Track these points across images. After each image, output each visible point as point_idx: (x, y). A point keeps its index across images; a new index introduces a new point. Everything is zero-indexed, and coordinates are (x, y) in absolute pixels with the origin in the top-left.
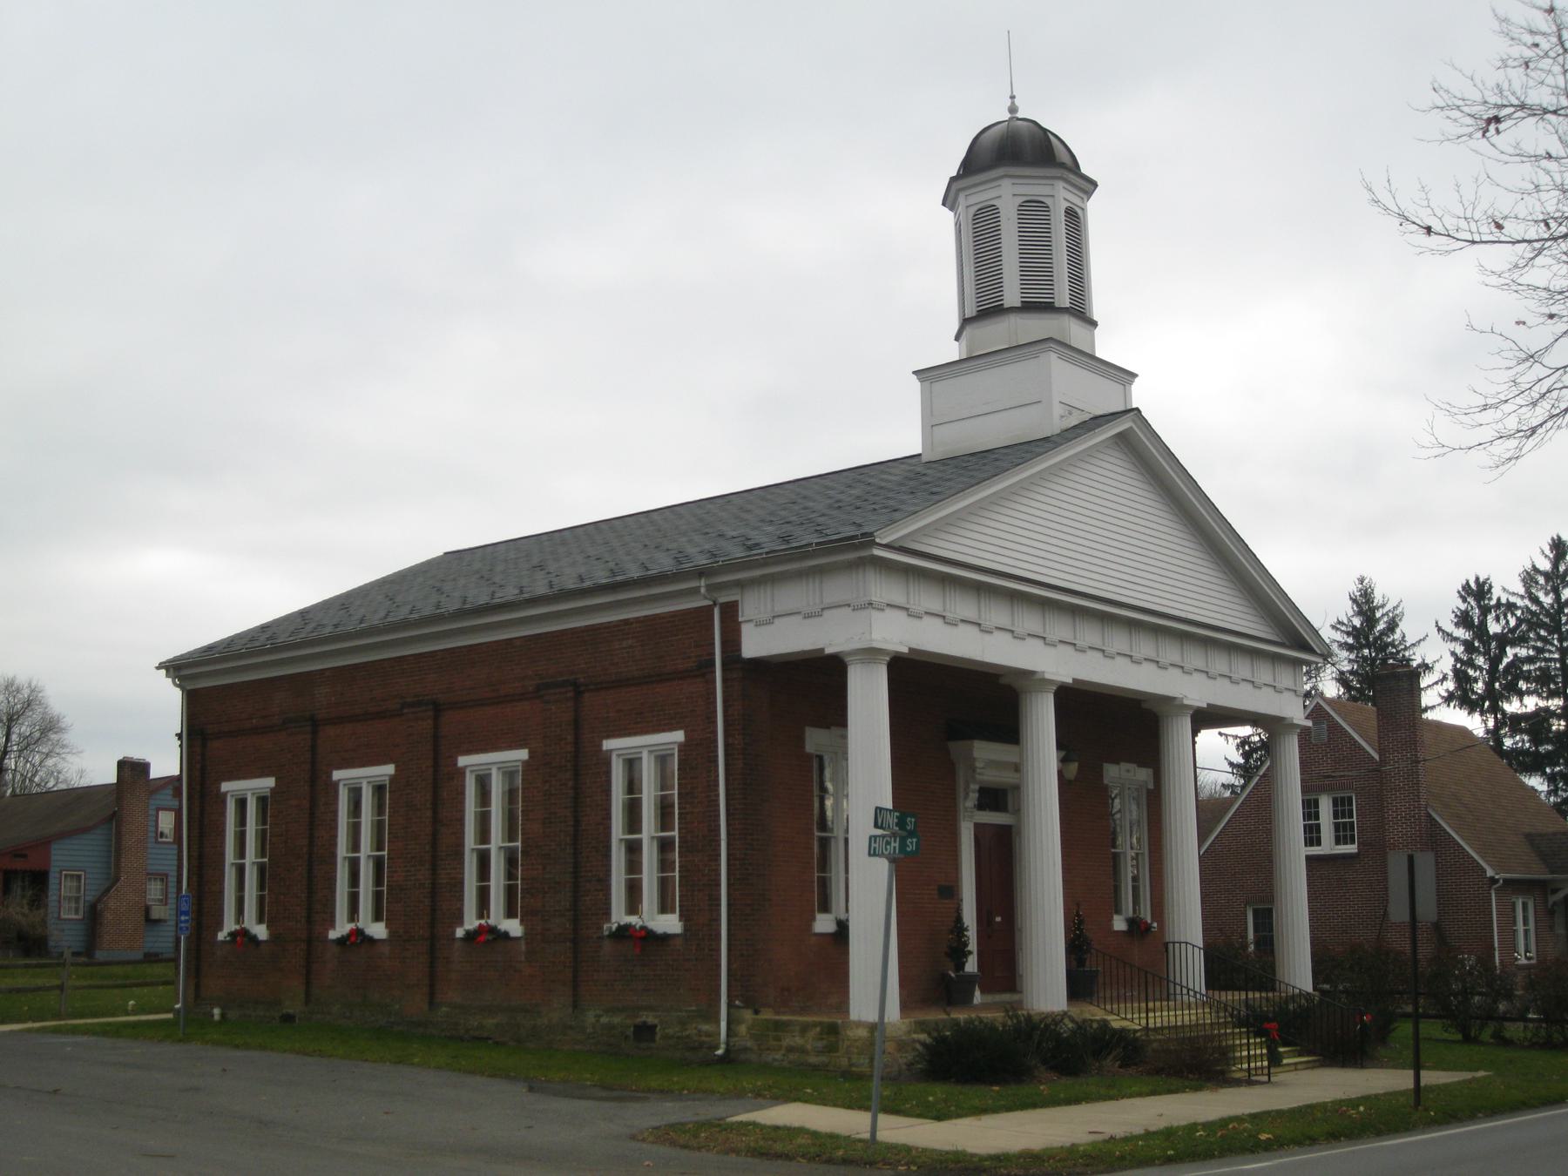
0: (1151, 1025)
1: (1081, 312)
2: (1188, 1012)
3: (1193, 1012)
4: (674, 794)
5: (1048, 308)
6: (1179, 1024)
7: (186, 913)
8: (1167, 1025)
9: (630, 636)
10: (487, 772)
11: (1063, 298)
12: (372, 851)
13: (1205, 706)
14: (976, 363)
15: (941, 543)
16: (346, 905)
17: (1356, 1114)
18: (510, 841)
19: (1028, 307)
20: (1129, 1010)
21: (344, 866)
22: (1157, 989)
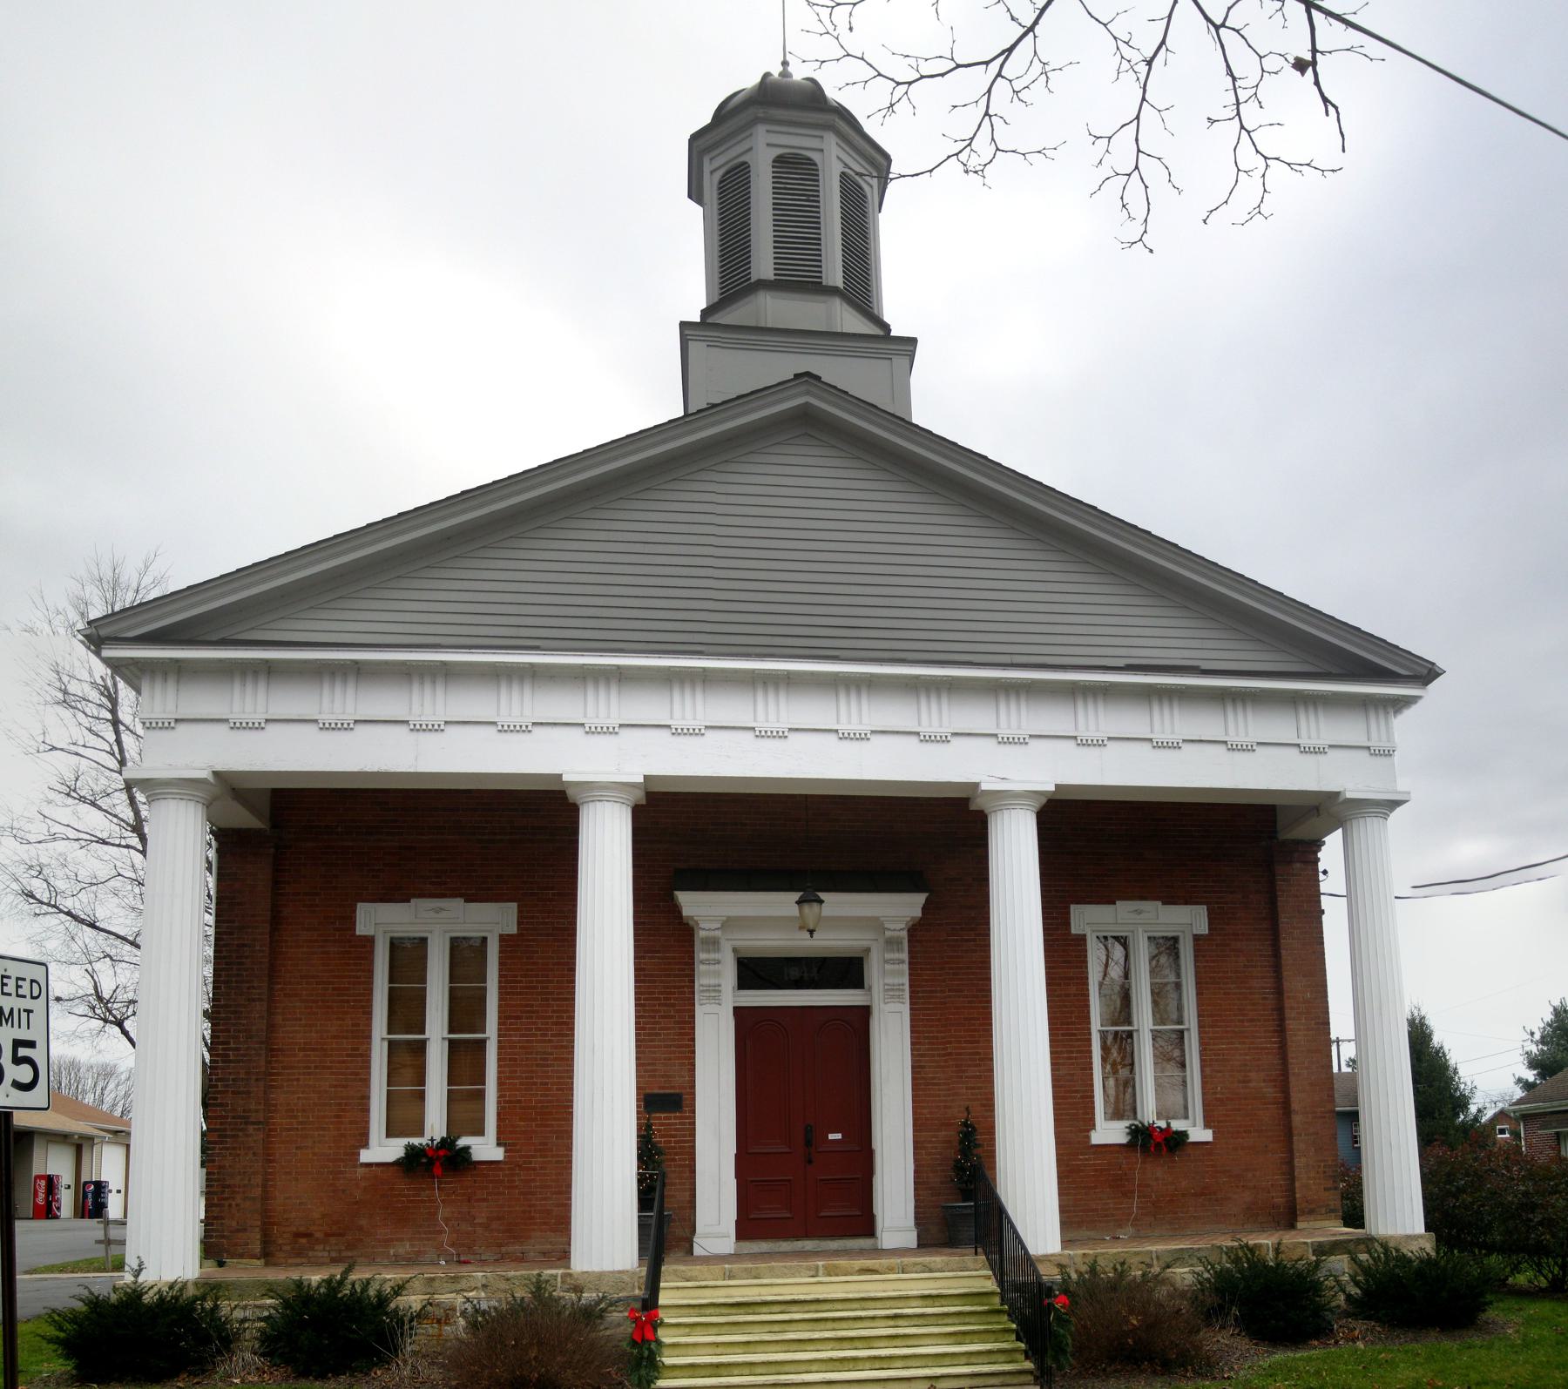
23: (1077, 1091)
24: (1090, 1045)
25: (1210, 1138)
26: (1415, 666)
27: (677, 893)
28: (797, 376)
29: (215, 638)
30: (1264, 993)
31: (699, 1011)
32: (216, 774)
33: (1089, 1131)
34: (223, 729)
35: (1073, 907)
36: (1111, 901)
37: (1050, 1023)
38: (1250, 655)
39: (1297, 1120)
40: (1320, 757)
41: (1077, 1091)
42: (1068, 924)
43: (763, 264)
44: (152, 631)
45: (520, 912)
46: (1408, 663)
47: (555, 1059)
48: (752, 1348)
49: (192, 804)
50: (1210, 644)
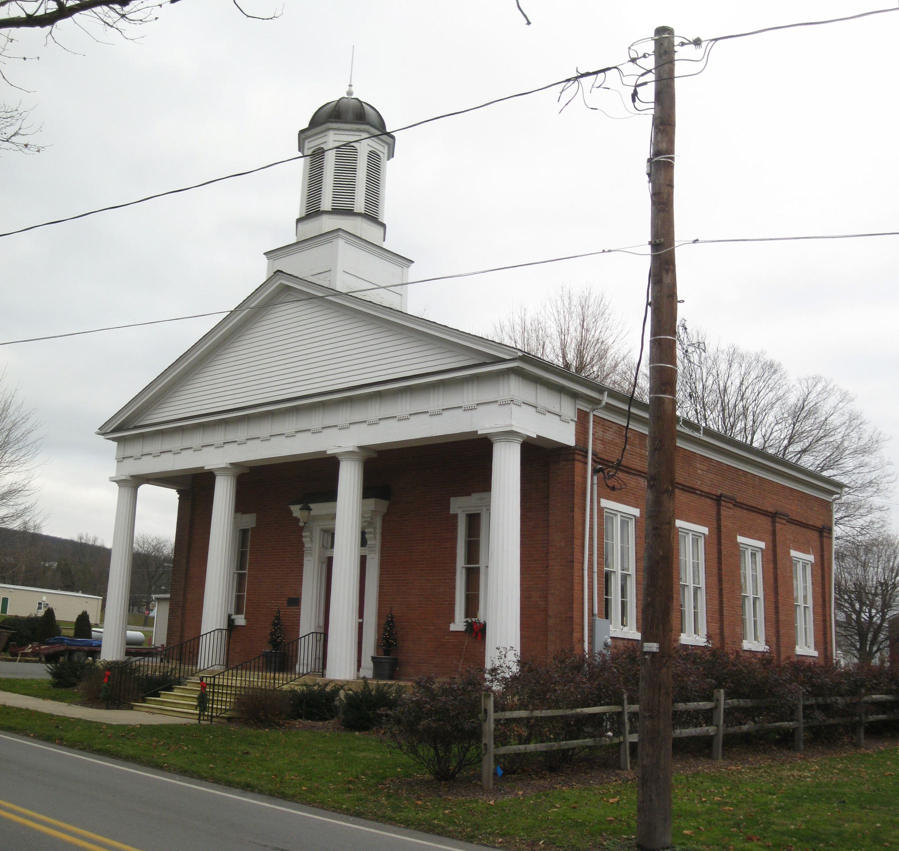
0: (216, 683)
1: (372, 217)
2: (235, 678)
3: (260, 680)
4: (247, 551)
5: (350, 213)
6: (263, 687)
7: (640, 600)
8: (239, 685)
9: (606, 399)
10: (479, 512)
11: (360, 205)
12: (237, 570)
13: (452, 512)
14: (363, 244)
15: (166, 414)
16: (233, 605)
17: (861, 767)
18: (240, 570)
19: (335, 211)
20: (252, 676)
21: (462, 574)
22: (154, 664)
23: (446, 601)
24: (455, 576)
25: (639, 638)
26: (513, 354)
27: (290, 506)
28: (275, 273)
29: (132, 427)
30: (543, 543)
31: (306, 559)
32: (360, 447)
33: (450, 623)
34: (364, 426)
35: (452, 499)
36: (469, 494)
37: (521, 564)
38: (453, 359)
39: (551, 621)
40: (473, 412)
41: (446, 601)
42: (449, 508)
43: (327, 204)
44: (116, 426)
45: (257, 517)
46: (511, 353)
47: (263, 582)
48: (184, 699)
49: (353, 462)
50: (429, 358)
